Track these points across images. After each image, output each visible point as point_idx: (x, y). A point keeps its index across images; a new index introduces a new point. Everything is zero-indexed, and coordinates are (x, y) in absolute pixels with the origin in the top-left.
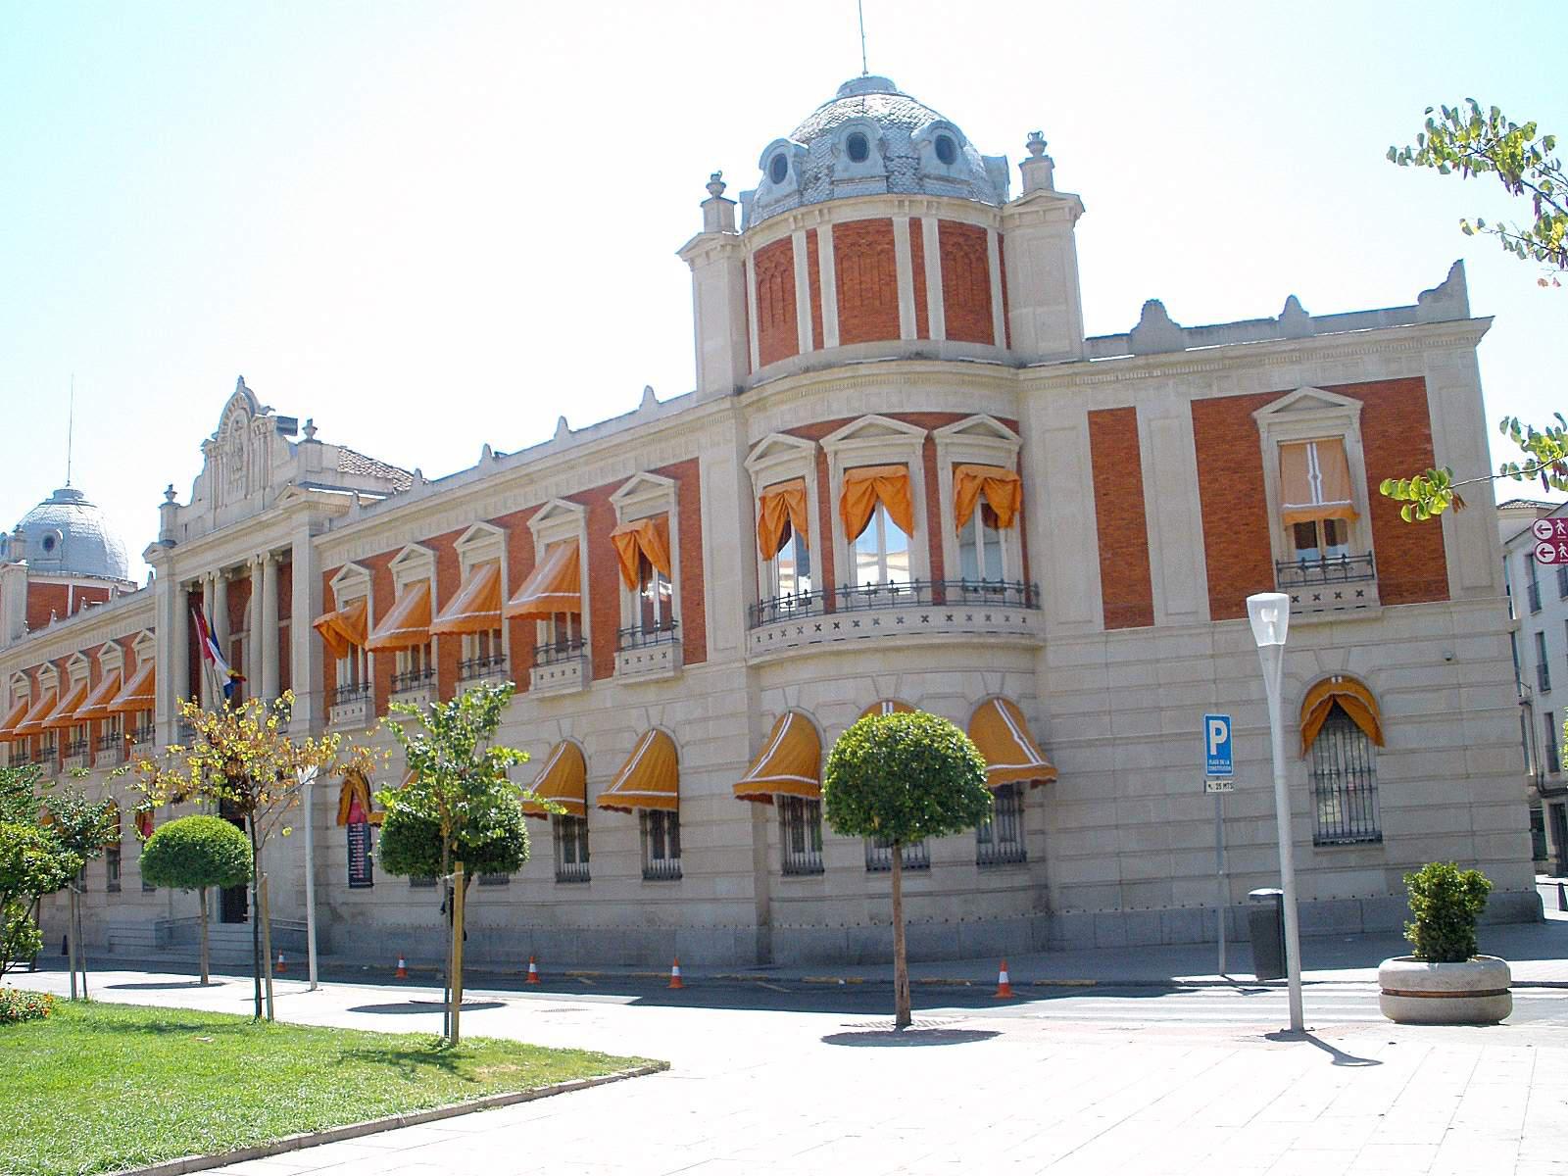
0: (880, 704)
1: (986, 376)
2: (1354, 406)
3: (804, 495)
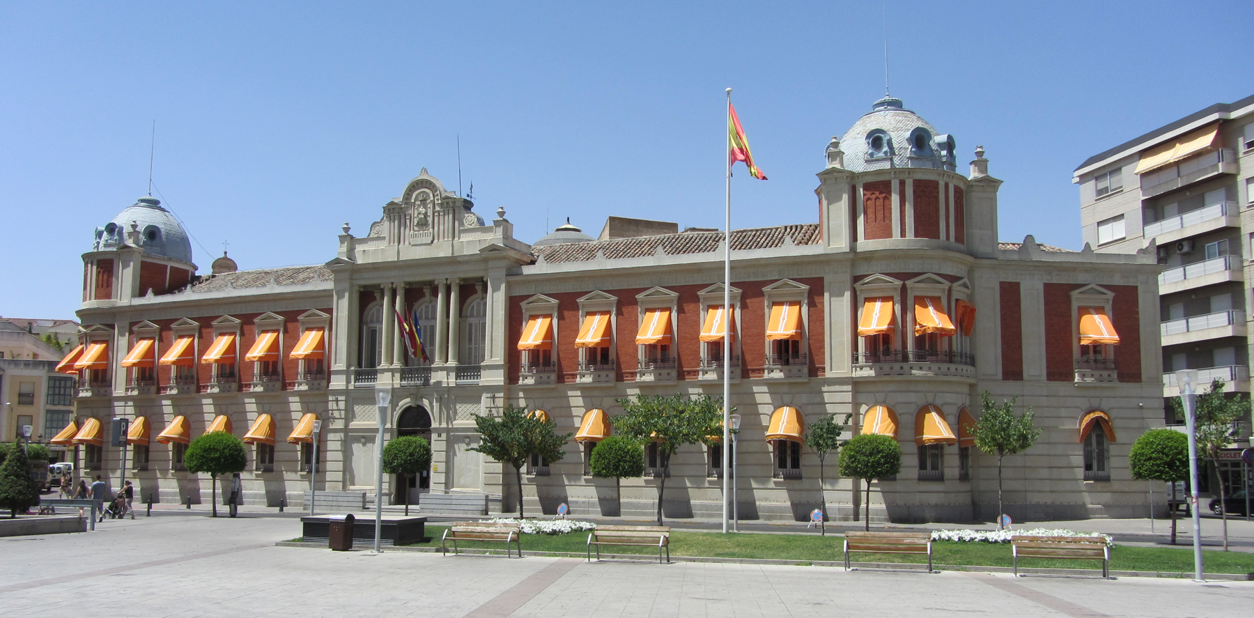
2: (1111, 295)
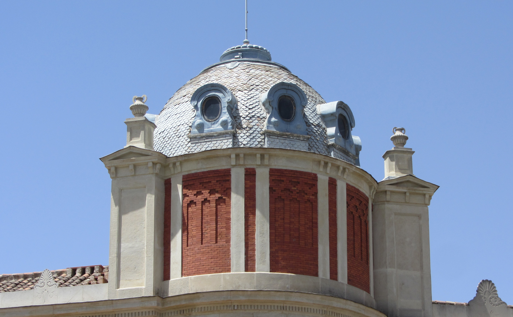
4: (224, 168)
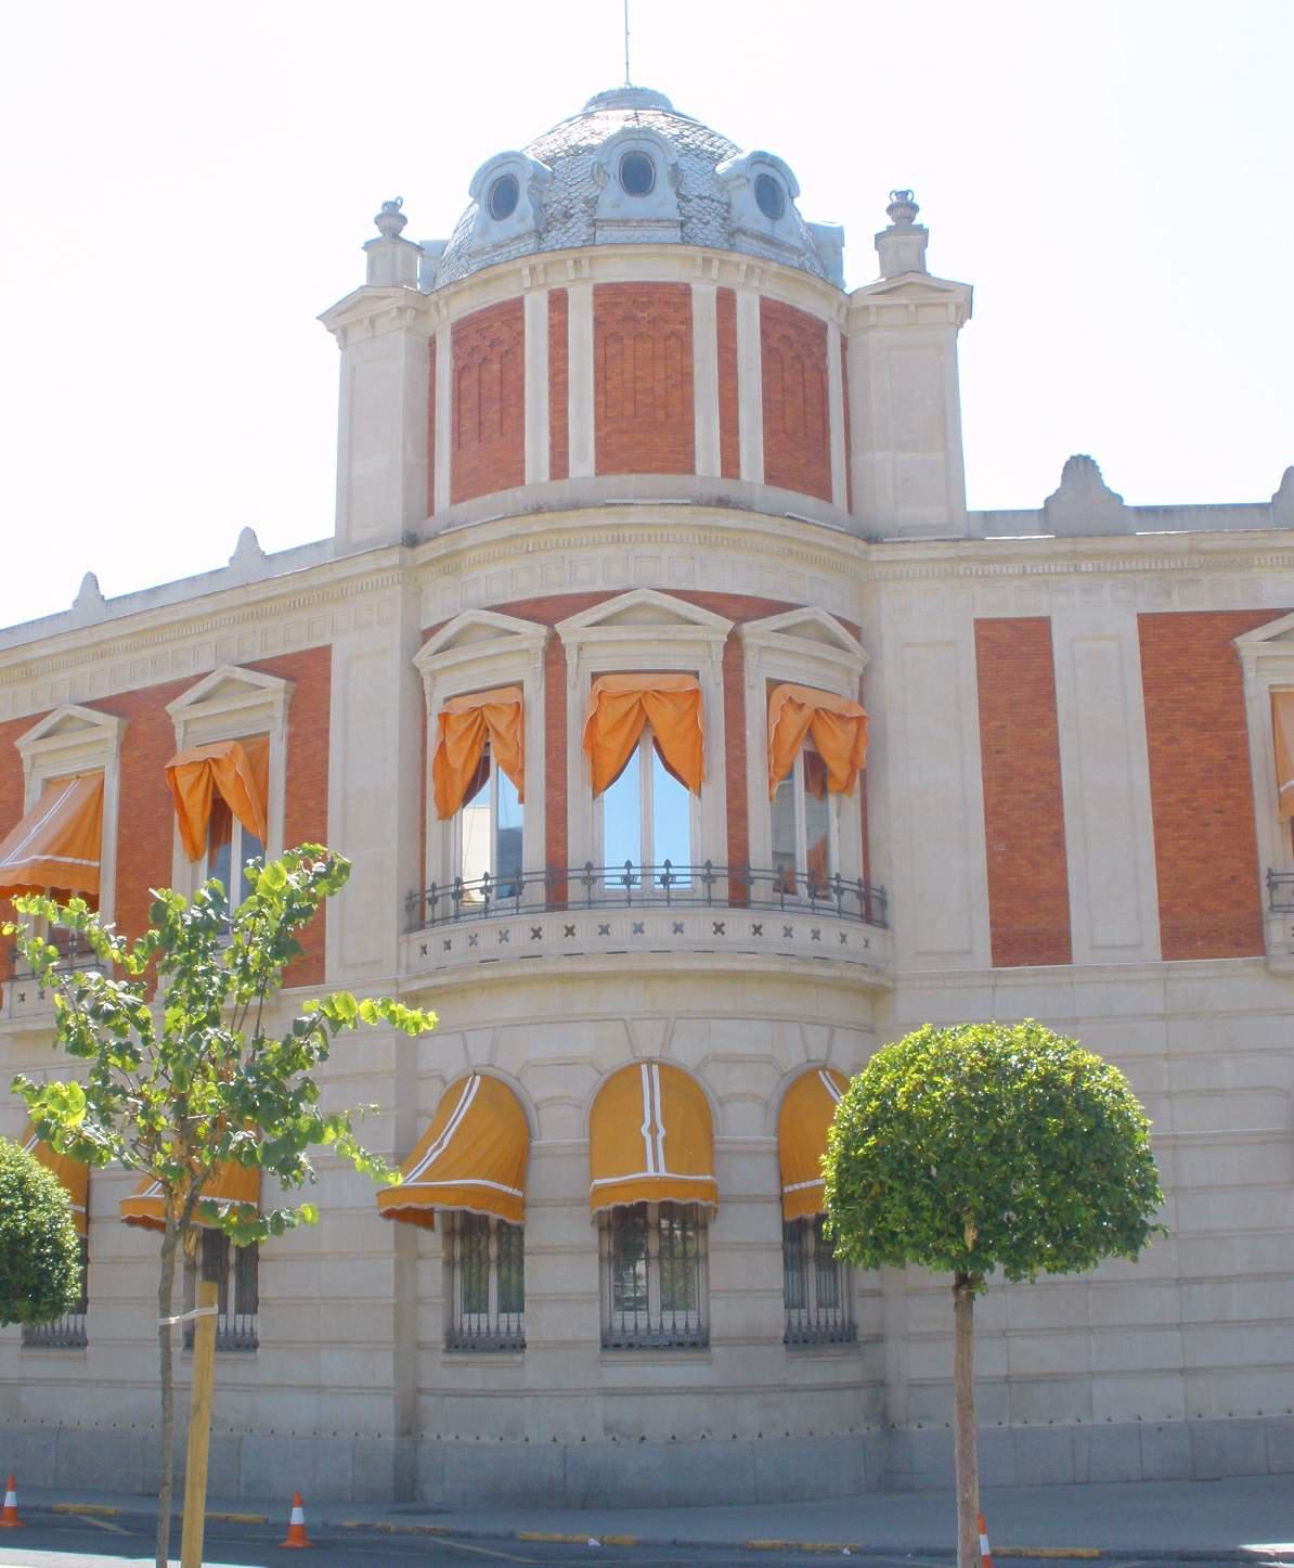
0: (639, 1064)
1: (821, 546)
3: (519, 710)
4: (513, 296)
